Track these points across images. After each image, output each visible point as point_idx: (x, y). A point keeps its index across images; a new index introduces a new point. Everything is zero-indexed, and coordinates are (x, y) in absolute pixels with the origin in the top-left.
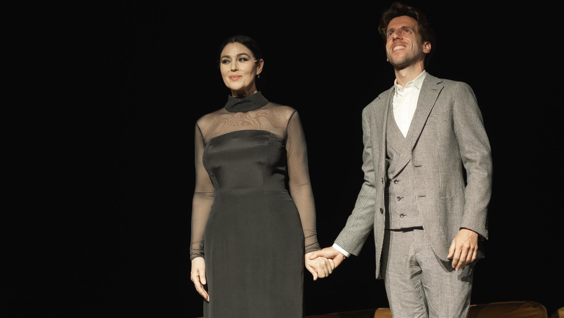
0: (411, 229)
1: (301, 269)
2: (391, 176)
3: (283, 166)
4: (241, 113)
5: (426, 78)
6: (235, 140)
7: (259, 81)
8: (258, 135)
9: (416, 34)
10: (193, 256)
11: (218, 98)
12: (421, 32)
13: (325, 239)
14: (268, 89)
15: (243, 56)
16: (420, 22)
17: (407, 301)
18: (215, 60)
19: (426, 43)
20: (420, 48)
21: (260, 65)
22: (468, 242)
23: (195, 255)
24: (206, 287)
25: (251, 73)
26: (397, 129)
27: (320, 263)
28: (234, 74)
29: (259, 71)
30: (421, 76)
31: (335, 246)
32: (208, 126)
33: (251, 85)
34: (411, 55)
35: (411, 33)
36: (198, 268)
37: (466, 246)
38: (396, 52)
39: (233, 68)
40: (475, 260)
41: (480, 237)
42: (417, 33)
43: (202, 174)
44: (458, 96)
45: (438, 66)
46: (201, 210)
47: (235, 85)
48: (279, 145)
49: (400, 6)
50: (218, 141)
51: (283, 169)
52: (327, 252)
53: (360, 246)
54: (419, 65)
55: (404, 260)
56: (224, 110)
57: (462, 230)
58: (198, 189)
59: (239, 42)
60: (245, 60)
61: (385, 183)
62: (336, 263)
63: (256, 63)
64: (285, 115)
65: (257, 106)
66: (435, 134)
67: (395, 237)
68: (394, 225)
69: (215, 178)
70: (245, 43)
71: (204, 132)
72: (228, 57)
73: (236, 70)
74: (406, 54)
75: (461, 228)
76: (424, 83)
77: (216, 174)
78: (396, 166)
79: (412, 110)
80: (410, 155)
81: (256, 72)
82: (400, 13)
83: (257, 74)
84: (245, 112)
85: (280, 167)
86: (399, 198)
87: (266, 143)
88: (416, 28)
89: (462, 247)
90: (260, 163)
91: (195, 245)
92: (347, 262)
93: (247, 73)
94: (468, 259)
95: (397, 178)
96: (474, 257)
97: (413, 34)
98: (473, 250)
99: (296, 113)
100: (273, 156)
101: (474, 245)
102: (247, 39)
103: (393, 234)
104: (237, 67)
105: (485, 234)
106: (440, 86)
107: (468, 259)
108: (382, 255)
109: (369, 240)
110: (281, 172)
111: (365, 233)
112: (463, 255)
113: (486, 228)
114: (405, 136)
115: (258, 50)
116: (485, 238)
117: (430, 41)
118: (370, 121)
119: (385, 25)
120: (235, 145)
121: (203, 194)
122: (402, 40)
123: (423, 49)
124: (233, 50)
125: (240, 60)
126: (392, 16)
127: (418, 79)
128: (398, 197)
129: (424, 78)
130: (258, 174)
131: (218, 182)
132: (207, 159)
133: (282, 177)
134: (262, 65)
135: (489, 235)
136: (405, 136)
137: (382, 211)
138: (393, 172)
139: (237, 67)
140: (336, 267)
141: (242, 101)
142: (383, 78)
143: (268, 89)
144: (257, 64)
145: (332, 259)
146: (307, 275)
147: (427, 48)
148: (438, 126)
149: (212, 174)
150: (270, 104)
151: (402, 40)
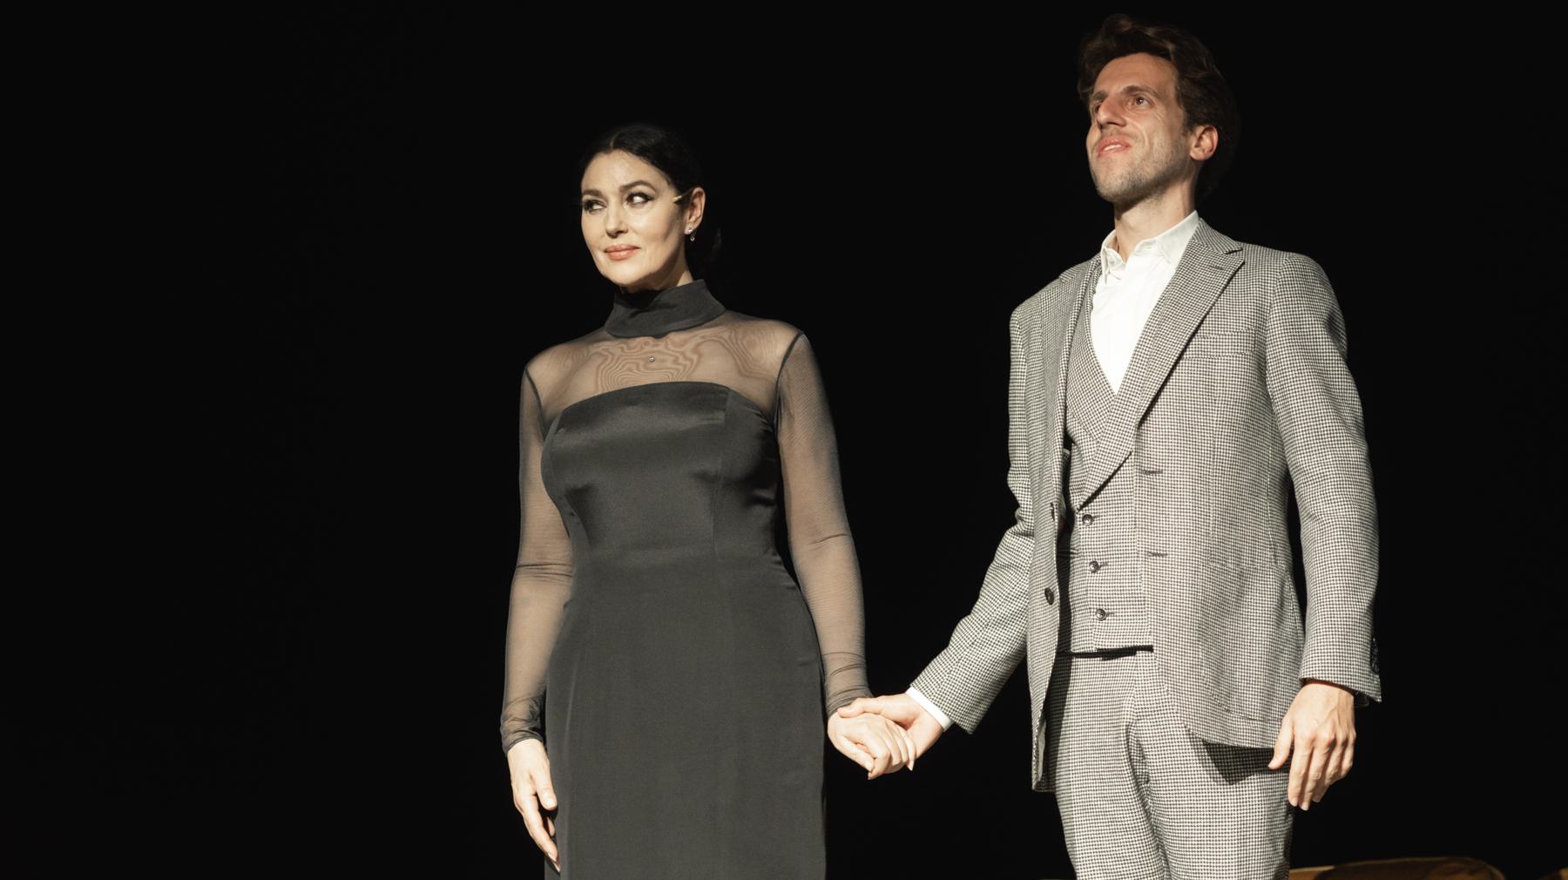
0: (1130, 651)
1: (820, 753)
2: (1076, 501)
3: (765, 486)
4: (650, 340)
5: (1197, 236)
6: (630, 409)
7: (692, 251)
8: (697, 396)
9: (1167, 106)
10: (511, 738)
11: (588, 305)
12: (1183, 98)
13: (891, 665)
14: (724, 272)
15: (640, 188)
16: (1183, 65)
17: (1119, 858)
18: (571, 202)
19: (1200, 129)
20: (1179, 148)
21: (694, 206)
22: (1329, 726)
23: (517, 736)
24: (546, 814)
25: (666, 236)
26: (1096, 370)
27: (885, 732)
28: (621, 241)
29: (692, 222)
30: (1183, 228)
31: (912, 692)
32: (550, 375)
33: (669, 267)
34: (1149, 172)
35: (1151, 104)
36: (530, 771)
37: (1325, 736)
38: (1112, 170)
39: (612, 227)
40: (1351, 771)
41: (1358, 697)
42: (1174, 105)
43: (540, 513)
44: (1283, 295)
45: (1232, 202)
46: (535, 616)
47: (624, 272)
48: (756, 425)
49: (1126, 25)
50: (584, 413)
51: (768, 494)
52: (891, 705)
53: (983, 707)
54: (1177, 196)
55: (1110, 740)
56: (604, 333)
57: (1311, 687)
58: (527, 554)
59: (629, 149)
60: (647, 198)
61: (1061, 518)
62: (912, 746)
63: (677, 202)
64: (773, 344)
65: (695, 318)
66: (1210, 388)
67: (1084, 674)
68: (1081, 641)
69: (577, 519)
70: (642, 153)
71: (544, 394)
72: (597, 193)
73: (615, 234)
74: (1131, 164)
75: (1305, 682)
76: (1190, 247)
77: (577, 505)
78: (1085, 478)
79: (1158, 345)
80: (1131, 445)
81: (683, 227)
82: (1128, 46)
83: (688, 231)
84: (659, 336)
85: (764, 478)
86: (1097, 567)
87: (720, 417)
88: (1171, 91)
89: (1313, 741)
90: (704, 478)
91: (517, 707)
92: (950, 738)
93: (652, 239)
94: (1331, 769)
95: (1091, 509)
96: (1347, 764)
97: (1160, 110)
98: (1345, 744)
99: (803, 341)
100: (739, 455)
101: (1346, 732)
102: (655, 135)
103: (1079, 663)
104: (630, 218)
105: (1371, 687)
106: (1236, 260)
107: (1331, 769)
108: (1047, 702)
109: (1011, 684)
110: (765, 502)
111: (1001, 669)
112: (1317, 762)
113: (1373, 670)
114: (1116, 388)
115: (679, 171)
116: (1372, 700)
117: (1211, 122)
118: (1027, 345)
119: (1091, 82)
120: (629, 423)
121: (539, 567)
122: (1136, 127)
123: (1188, 150)
124: (612, 171)
125: (630, 199)
126: (1107, 56)
127: (1172, 234)
128: (1095, 563)
129: (1190, 233)
130: (696, 510)
131: (587, 530)
132: (554, 467)
133: (763, 514)
134: (700, 203)
135: (1385, 687)
136: (1116, 388)
137: (1049, 595)
138: (1081, 490)
139: (630, 218)
140: (919, 753)
141: (644, 306)
142: (1077, 226)
143: (724, 272)
144: (684, 205)
145: (904, 725)
146: (840, 768)
147: (1204, 144)
148: (1220, 366)
149: (569, 509)
150: (728, 314)
151: (1136, 127)
